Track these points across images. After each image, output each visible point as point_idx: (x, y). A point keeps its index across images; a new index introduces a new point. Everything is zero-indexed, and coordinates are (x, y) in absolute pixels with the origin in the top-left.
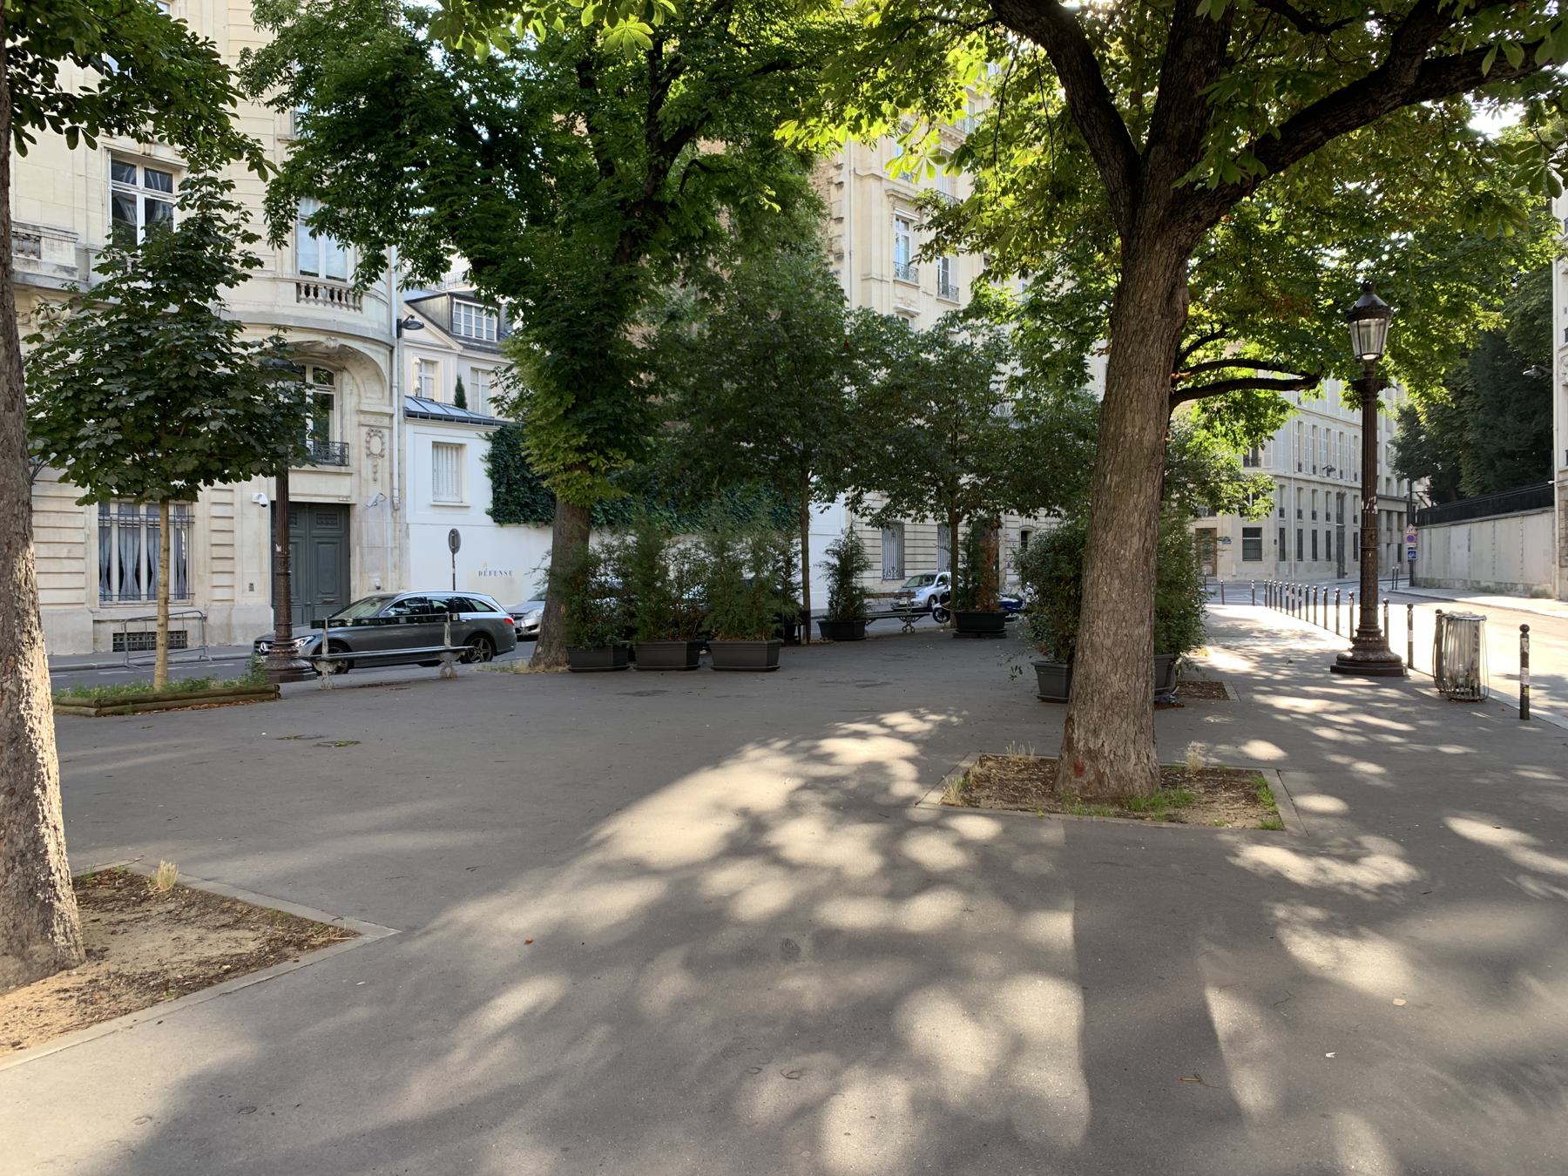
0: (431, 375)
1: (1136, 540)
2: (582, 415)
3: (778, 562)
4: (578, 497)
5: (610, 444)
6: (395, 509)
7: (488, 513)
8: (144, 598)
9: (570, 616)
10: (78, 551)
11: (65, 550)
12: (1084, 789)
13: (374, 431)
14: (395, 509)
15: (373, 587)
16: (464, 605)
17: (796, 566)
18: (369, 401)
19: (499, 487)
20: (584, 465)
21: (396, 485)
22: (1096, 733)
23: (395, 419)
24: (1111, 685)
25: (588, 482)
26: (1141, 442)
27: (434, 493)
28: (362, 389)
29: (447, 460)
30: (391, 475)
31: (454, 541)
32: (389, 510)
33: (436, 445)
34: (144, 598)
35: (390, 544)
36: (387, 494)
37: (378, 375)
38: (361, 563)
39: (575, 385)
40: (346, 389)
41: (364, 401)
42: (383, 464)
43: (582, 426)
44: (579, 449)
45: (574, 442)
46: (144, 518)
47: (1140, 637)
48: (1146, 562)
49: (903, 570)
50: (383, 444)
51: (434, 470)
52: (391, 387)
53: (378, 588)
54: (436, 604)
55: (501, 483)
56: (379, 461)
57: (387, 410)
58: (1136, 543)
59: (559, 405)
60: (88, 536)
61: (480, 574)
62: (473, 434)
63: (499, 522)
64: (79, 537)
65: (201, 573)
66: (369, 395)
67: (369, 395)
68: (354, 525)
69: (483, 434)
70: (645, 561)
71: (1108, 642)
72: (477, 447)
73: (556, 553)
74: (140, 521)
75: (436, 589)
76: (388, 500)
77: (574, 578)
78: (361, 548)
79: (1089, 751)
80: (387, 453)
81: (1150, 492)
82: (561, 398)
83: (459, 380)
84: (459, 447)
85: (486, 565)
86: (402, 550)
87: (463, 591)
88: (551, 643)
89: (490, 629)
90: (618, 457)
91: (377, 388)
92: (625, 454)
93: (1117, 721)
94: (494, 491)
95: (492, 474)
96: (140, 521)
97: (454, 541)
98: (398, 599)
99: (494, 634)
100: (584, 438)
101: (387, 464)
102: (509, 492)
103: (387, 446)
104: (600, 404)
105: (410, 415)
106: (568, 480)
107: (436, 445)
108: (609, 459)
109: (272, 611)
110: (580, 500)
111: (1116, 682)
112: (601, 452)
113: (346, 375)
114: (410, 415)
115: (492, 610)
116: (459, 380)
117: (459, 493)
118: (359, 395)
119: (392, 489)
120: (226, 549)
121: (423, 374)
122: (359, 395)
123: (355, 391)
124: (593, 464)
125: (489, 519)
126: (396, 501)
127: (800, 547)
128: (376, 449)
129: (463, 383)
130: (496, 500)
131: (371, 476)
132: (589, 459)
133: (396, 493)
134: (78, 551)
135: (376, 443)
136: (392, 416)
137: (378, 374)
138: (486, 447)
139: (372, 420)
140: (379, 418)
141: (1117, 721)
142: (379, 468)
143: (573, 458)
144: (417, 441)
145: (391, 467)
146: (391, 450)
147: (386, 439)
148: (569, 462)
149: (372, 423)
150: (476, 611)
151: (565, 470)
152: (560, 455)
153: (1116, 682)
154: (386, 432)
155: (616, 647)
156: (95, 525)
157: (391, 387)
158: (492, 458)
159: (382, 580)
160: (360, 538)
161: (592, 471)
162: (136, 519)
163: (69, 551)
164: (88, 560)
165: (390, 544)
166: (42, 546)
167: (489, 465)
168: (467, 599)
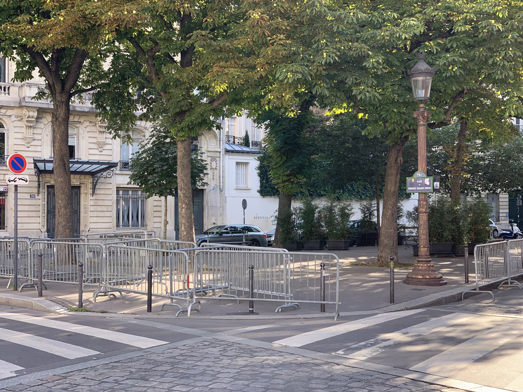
0: (234, 124)
1: (390, 211)
2: (288, 164)
3: (366, 214)
4: (287, 192)
5: (298, 173)
6: (221, 191)
7: (258, 192)
8: (130, 226)
9: (283, 232)
10: (110, 209)
11: (106, 208)
12: (379, 264)
13: (213, 159)
14: (221, 191)
15: (212, 223)
16: (249, 229)
17: (374, 215)
18: (211, 147)
19: (262, 180)
20: (289, 180)
21: (221, 181)
22: (382, 252)
23: (221, 153)
24: (384, 242)
25: (290, 186)
26: (391, 190)
27: (236, 184)
28: (209, 142)
29: (242, 169)
30: (220, 176)
31: (244, 204)
32: (218, 191)
33: (237, 163)
34: (130, 226)
35: (219, 206)
36: (218, 185)
37: (215, 136)
38: (208, 213)
39: (286, 153)
40: (203, 142)
41: (209, 147)
42: (216, 172)
43: (288, 168)
44: (287, 175)
45: (285, 173)
46: (121, 196)
47: (391, 232)
48: (393, 216)
49: (499, 217)
50: (216, 164)
51: (236, 174)
52: (220, 140)
53: (214, 224)
54: (239, 229)
55: (264, 179)
56: (215, 171)
57: (219, 150)
58: (390, 212)
59: (281, 160)
60: (113, 203)
61: (255, 218)
62: (252, 158)
63: (263, 195)
64: (110, 203)
65: (150, 217)
66: (212, 144)
67: (212, 144)
68: (205, 198)
69: (256, 158)
70: (308, 212)
71: (384, 233)
72: (254, 163)
73: (280, 210)
74: (130, 197)
75: (239, 224)
76: (218, 187)
77: (284, 219)
78: (208, 207)
79: (381, 256)
80: (218, 168)
81: (393, 201)
82: (281, 158)
83: (247, 132)
84: (246, 164)
85: (257, 214)
86: (223, 208)
87: (248, 224)
88: (278, 242)
89: (258, 238)
90: (301, 178)
91: (214, 141)
92: (303, 177)
93: (386, 250)
94: (261, 182)
95: (260, 175)
96: (130, 197)
97: (244, 204)
98: (226, 227)
99: (259, 240)
100: (289, 172)
101: (218, 172)
102: (267, 182)
103: (218, 165)
104: (294, 160)
105: (227, 151)
106: (284, 186)
107: (237, 163)
108: (297, 178)
109: (175, 232)
110: (288, 193)
111: (386, 242)
112: (295, 176)
113: (203, 136)
114: (227, 151)
115: (259, 232)
116: (247, 132)
117: (246, 184)
118: (208, 145)
119: (220, 183)
120: (159, 207)
121: (230, 123)
122: (208, 145)
123: (206, 143)
124: (292, 180)
125: (259, 194)
126: (221, 188)
127: (376, 208)
128: (214, 167)
129: (248, 133)
130: (261, 186)
131: (212, 177)
132: (291, 179)
133: (221, 184)
134: (110, 209)
135: (214, 163)
136: (220, 152)
137: (215, 135)
138: (257, 163)
139: (212, 154)
140: (215, 153)
141: (386, 250)
142: (215, 174)
143: (285, 178)
144: (230, 161)
145: (220, 173)
146: (220, 166)
147: (218, 162)
148: (284, 180)
149: (212, 156)
150: (253, 232)
151: (283, 182)
152: (281, 177)
153: (386, 242)
154: (218, 159)
155: (297, 242)
156: (115, 198)
157: (220, 140)
158: (260, 168)
159: (216, 220)
160: (207, 203)
161: (292, 183)
162: (137, 196)
163: (107, 209)
164: (113, 212)
165: (219, 206)
166: (99, 207)
167: (259, 171)
168: (250, 227)
